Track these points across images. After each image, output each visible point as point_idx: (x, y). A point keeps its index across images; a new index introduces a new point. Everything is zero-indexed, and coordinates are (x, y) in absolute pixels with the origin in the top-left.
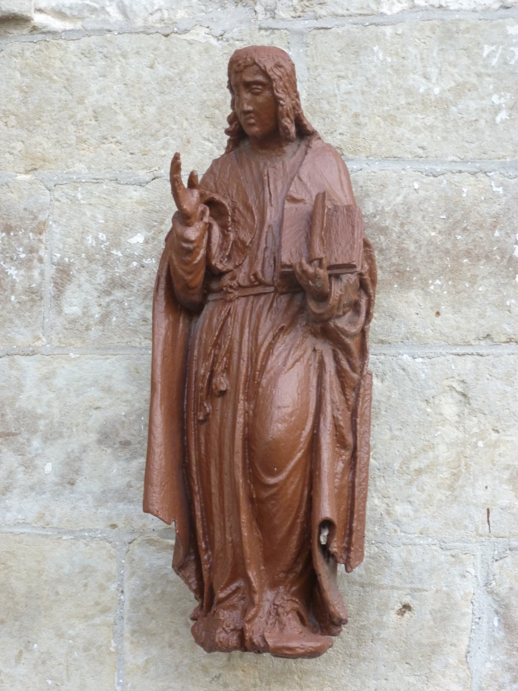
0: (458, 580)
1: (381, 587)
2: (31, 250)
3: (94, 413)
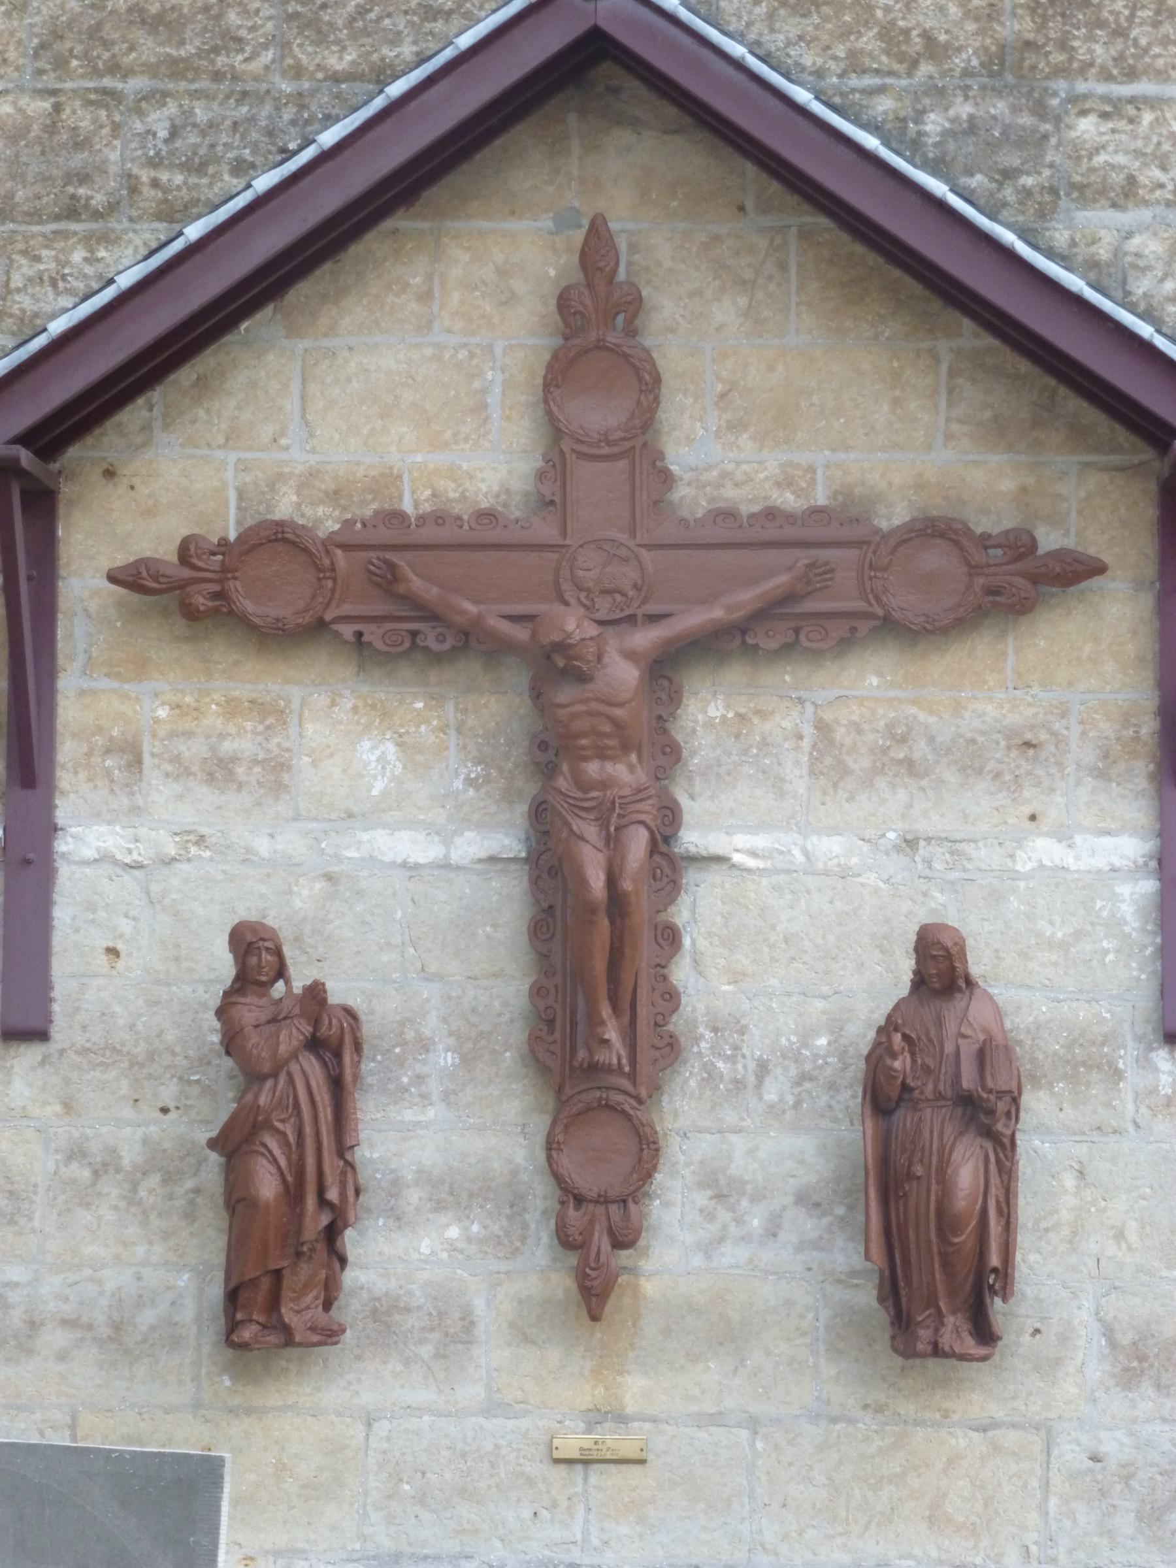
0: (1075, 1311)
1: (1018, 1316)
2: (736, 1048)
3: (791, 1180)
